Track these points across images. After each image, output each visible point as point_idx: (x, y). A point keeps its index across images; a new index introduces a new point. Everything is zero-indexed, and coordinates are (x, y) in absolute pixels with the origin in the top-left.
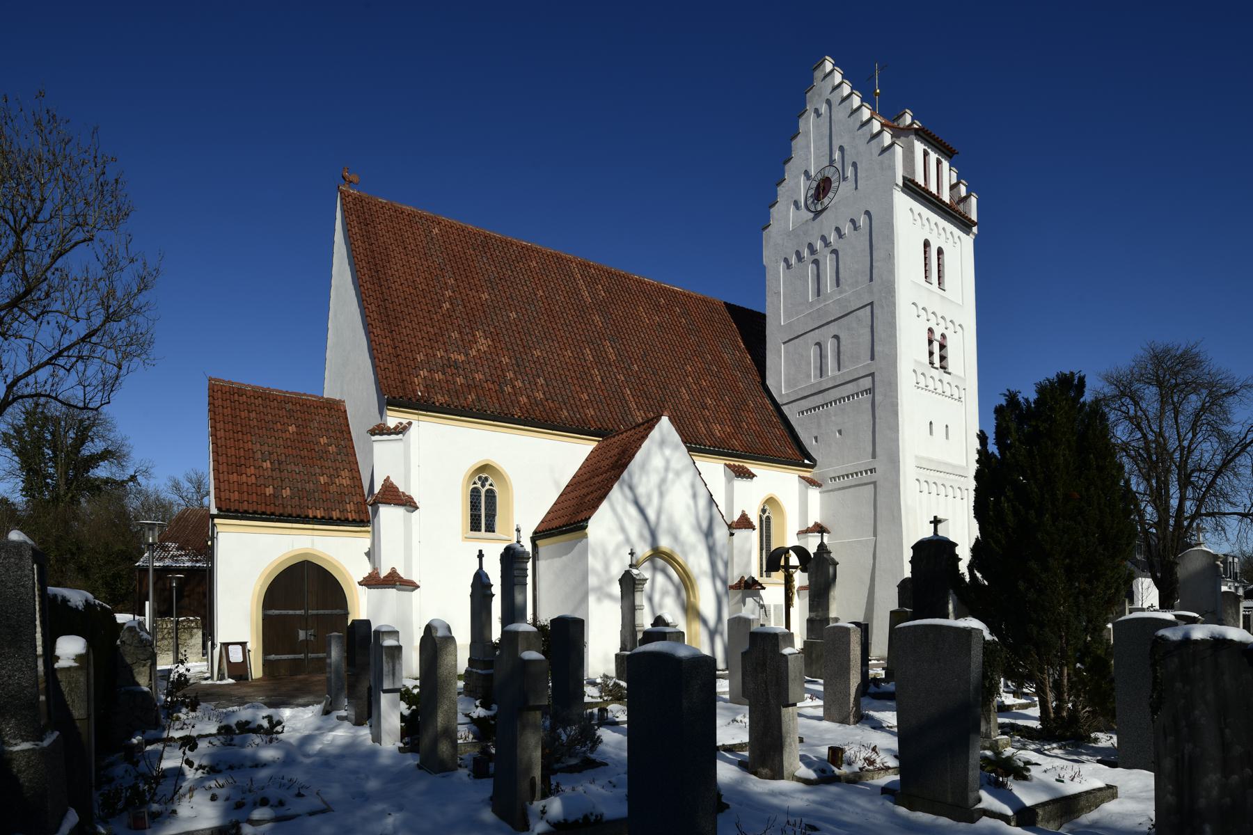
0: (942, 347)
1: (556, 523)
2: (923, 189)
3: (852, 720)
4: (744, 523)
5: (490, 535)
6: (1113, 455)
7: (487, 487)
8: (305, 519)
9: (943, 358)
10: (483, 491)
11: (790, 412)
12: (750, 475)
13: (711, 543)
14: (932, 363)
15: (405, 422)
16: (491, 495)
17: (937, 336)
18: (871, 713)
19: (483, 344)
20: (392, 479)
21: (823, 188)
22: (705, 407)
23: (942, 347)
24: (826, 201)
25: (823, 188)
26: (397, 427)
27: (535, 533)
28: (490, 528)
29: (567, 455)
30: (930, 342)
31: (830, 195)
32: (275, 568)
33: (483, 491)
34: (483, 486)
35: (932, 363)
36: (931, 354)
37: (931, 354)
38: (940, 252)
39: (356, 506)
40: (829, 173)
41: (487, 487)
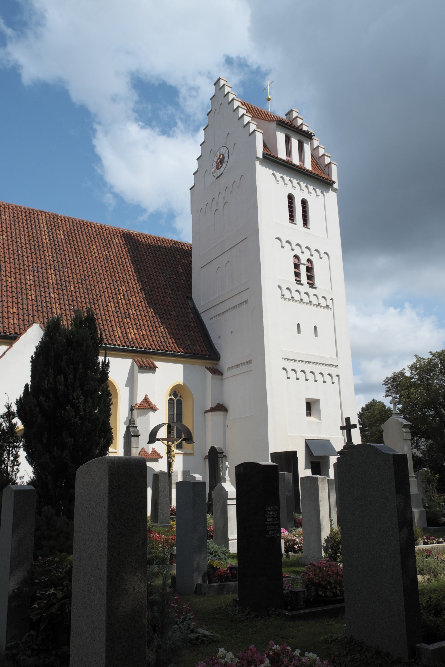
24: (222, 170)
30: (296, 266)
36: (297, 275)
37: (297, 275)
40: (224, 151)
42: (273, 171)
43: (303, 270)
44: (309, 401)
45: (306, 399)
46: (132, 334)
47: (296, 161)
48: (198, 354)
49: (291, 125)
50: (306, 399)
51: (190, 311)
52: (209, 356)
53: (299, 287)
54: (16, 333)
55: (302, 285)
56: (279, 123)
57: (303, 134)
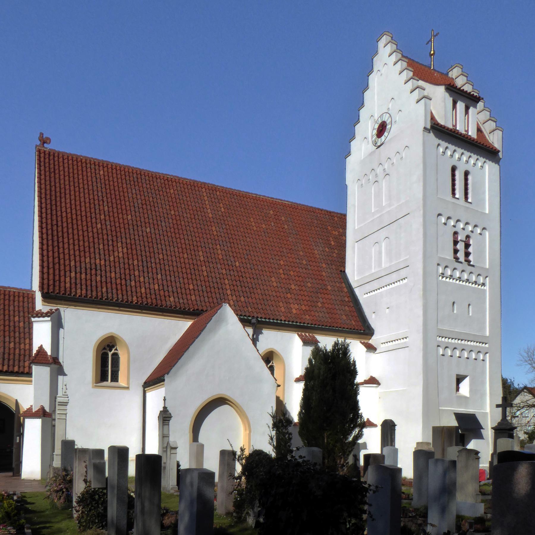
0: (467, 246)
3: (454, 443)
5: (114, 384)
6: (427, 526)
9: (467, 254)
10: (110, 354)
11: (357, 291)
13: (165, 432)
16: (116, 358)
19: (121, 251)
20: (44, 347)
21: (382, 129)
23: (467, 246)
24: (383, 138)
25: (382, 129)
26: (48, 312)
27: (145, 383)
28: (115, 378)
29: (183, 325)
30: (456, 243)
31: (386, 134)
32: (9, 396)
35: (457, 259)
36: (456, 251)
37: (456, 251)
38: (467, 174)
40: (386, 118)
42: (477, 155)
43: (461, 246)
44: (458, 377)
45: (457, 375)
46: (295, 309)
47: (460, 128)
48: (354, 329)
49: (453, 85)
50: (457, 375)
51: (344, 286)
52: (364, 331)
53: (457, 265)
54: (202, 310)
55: (461, 263)
56: (449, 87)
57: (461, 93)
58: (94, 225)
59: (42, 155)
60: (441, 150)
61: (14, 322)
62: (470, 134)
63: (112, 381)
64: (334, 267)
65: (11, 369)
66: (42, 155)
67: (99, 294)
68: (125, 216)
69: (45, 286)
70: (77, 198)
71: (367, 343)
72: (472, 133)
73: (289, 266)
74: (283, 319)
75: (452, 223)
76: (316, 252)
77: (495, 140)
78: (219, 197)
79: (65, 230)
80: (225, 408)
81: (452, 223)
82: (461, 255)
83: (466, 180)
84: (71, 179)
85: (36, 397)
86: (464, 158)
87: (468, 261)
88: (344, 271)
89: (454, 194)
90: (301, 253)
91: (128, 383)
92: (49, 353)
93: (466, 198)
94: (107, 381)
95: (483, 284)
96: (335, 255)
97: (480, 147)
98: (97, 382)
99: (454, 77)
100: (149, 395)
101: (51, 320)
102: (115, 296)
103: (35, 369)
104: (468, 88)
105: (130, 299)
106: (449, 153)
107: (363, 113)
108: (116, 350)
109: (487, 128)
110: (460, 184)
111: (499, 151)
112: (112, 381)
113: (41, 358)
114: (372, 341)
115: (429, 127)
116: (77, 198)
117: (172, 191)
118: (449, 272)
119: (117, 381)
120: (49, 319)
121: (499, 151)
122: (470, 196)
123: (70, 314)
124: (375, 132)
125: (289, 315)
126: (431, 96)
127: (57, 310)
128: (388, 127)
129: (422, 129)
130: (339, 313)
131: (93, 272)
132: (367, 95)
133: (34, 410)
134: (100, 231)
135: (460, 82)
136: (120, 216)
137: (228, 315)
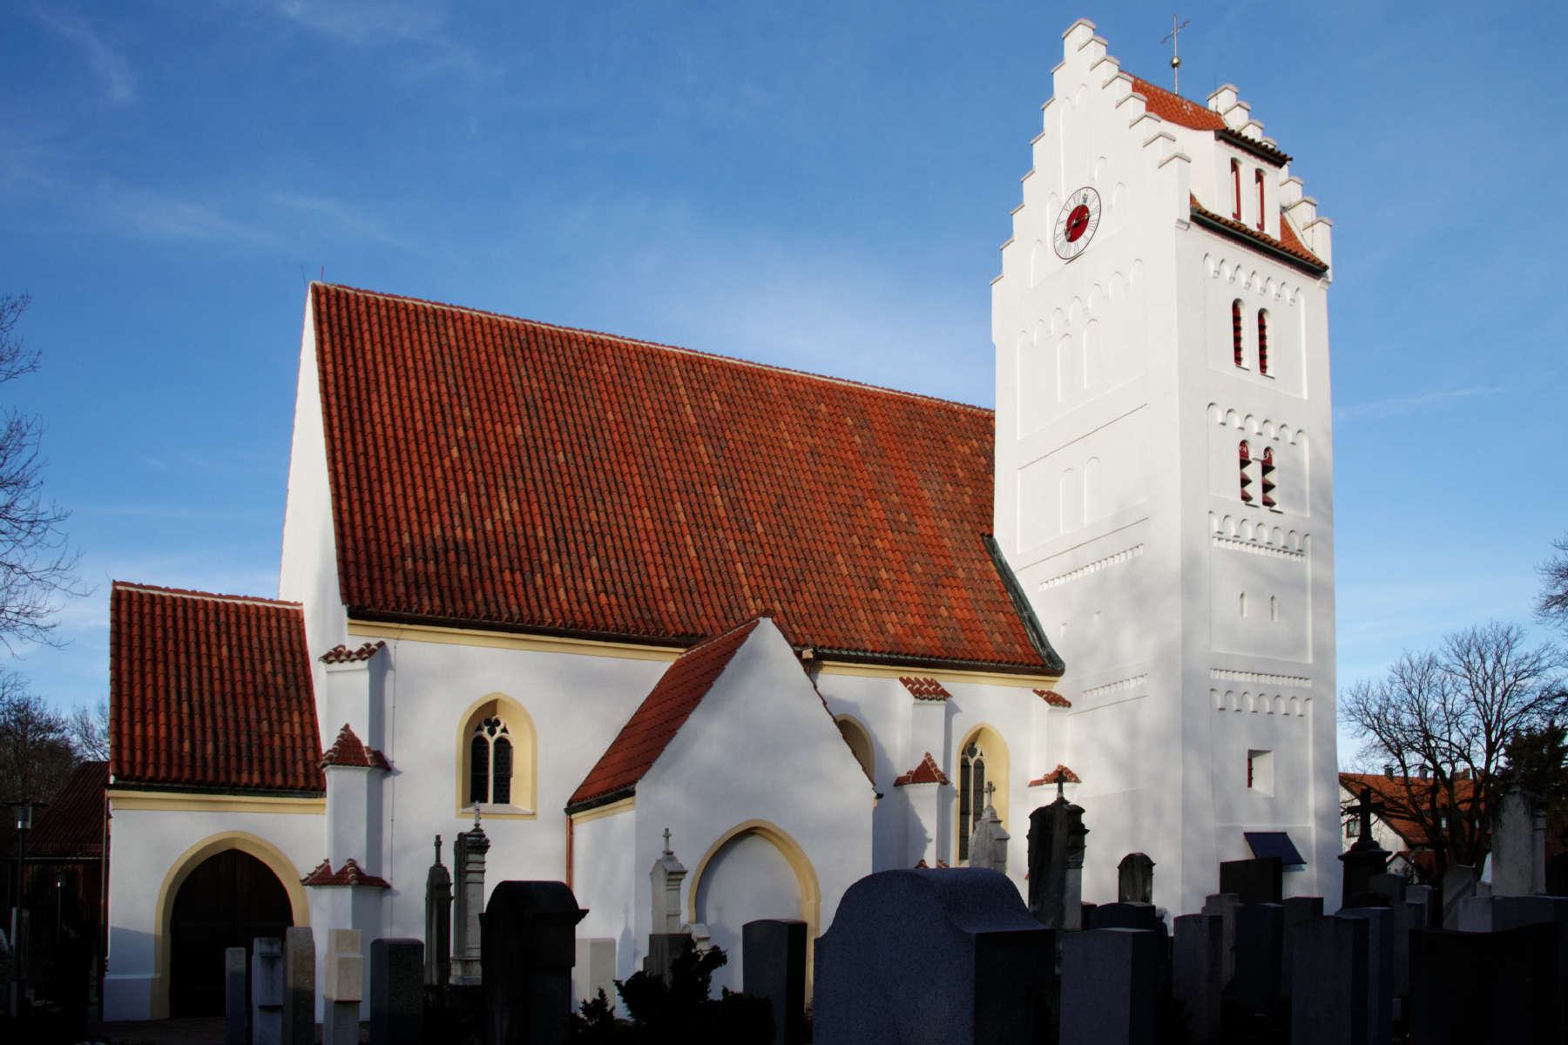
0: (1267, 467)
1: (599, 786)
2: (1257, 237)
4: (925, 773)
5: (501, 807)
7: (498, 734)
8: (235, 789)
9: (1267, 487)
10: (491, 741)
12: (990, 784)
14: (1246, 498)
15: (374, 642)
16: (504, 747)
17: (1255, 453)
18: (1024, 890)
20: (353, 729)
21: (1077, 223)
22: (876, 584)
23: (1267, 467)
24: (1081, 241)
25: (1077, 223)
27: (570, 803)
28: (503, 796)
29: (648, 668)
30: (1244, 462)
31: (1088, 232)
32: (194, 857)
33: (491, 741)
34: (492, 732)
35: (1246, 498)
37: (1245, 482)
39: (293, 771)
41: (498, 734)
43: (1254, 471)
47: (1249, 221)
58: (445, 452)
59: (323, 299)
60: (1212, 265)
61: (265, 676)
62: (1267, 231)
63: (495, 802)
64: (968, 527)
65: (268, 781)
66: (323, 299)
67: (471, 605)
68: (509, 429)
69: (355, 592)
70: (405, 393)
71: (1049, 693)
72: (1273, 231)
73: (883, 528)
74: (870, 647)
75: (1237, 421)
76: (927, 495)
77: (1317, 242)
78: (708, 378)
79: (384, 465)
80: (754, 845)
81: (1237, 421)
82: (1255, 490)
83: (1262, 327)
84: (388, 350)
85: (338, 840)
86: (1258, 283)
87: (1268, 503)
88: (991, 536)
89: (1238, 359)
90: (895, 499)
91: (534, 805)
92: (365, 743)
93: (1263, 367)
94: (485, 801)
95: (1300, 552)
96: (967, 500)
97: (1288, 254)
98: (464, 806)
99: (1221, 111)
100: (577, 828)
101: (370, 668)
102: (504, 608)
103: (332, 776)
104: (1253, 133)
105: (537, 614)
106: (1227, 271)
107: (1031, 187)
108: (504, 730)
109: (1301, 217)
110: (1249, 337)
111: (1326, 268)
112: (495, 802)
113: (349, 753)
114: (1059, 686)
115: (1187, 218)
116: (405, 393)
117: (605, 369)
118: (1232, 529)
119: (507, 802)
120: (365, 664)
121: (1326, 268)
122: (1269, 362)
123: (415, 649)
124: (1063, 227)
125: (882, 639)
126: (1188, 154)
127: (381, 645)
128: (1093, 218)
129: (1174, 222)
130: (987, 628)
131: (452, 555)
132: (1039, 149)
133: (334, 871)
134: (458, 465)
135: (1236, 120)
136: (499, 428)
137: (769, 638)
